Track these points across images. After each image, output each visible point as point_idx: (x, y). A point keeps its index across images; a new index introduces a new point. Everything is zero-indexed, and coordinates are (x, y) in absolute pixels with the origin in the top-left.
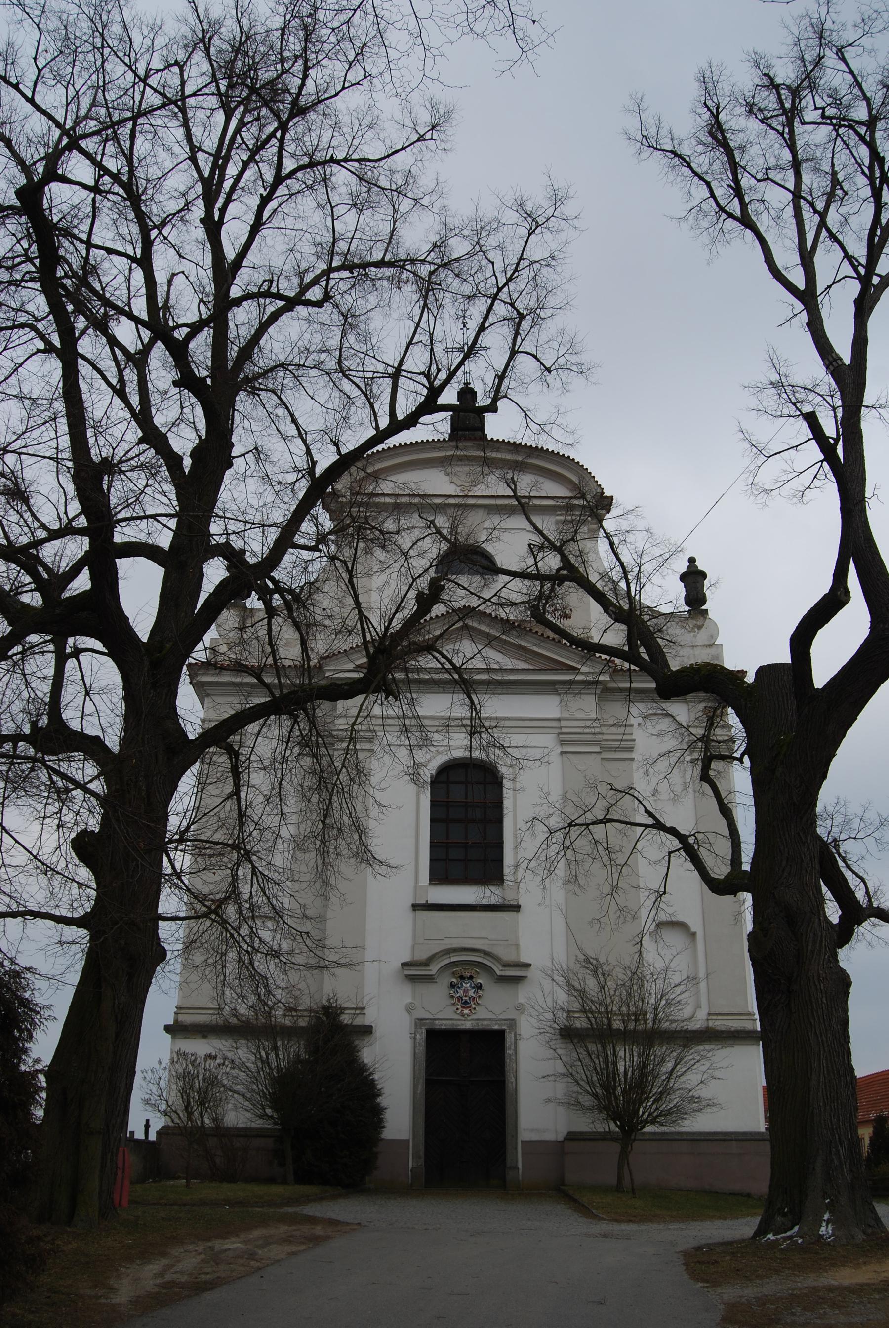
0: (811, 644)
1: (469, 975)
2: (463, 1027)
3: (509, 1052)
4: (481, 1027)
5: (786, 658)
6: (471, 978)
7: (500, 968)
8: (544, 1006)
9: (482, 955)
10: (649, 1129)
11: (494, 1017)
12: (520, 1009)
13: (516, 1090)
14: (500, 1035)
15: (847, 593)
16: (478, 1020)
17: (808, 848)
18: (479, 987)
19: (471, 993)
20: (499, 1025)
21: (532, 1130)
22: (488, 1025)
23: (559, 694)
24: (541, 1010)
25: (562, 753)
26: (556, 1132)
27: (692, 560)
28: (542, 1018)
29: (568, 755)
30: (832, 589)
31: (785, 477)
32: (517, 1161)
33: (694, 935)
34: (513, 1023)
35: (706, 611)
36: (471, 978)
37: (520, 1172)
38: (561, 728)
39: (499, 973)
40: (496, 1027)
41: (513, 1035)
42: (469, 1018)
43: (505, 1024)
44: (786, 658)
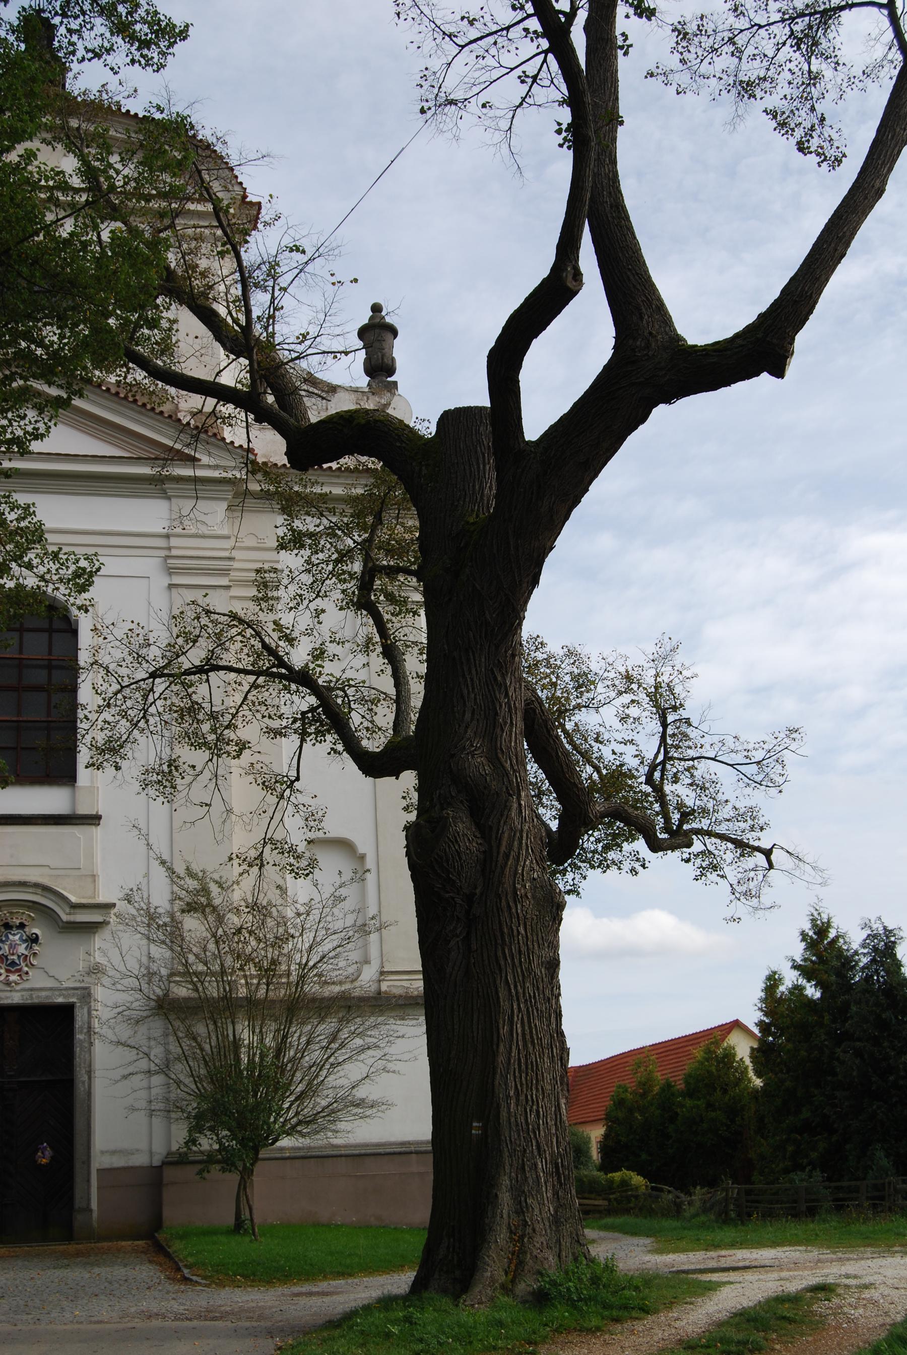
0: (522, 360)
1: (18, 922)
2: (9, 1001)
3: (79, 1036)
4: (36, 1001)
5: (481, 398)
6: (22, 926)
7: (68, 910)
8: (122, 968)
9: (39, 891)
10: (285, 1142)
11: (56, 985)
12: (96, 970)
13: (89, 1094)
14: (65, 1013)
15: (578, 275)
16: (32, 990)
17: (507, 695)
18: (34, 940)
19: (22, 949)
20: (65, 997)
21: (114, 1152)
22: (47, 997)
23: (169, 498)
24: (118, 975)
25: (171, 586)
26: (151, 1153)
27: (376, 309)
28: (119, 987)
29: (181, 590)
30: (554, 269)
31: (487, 77)
32: (89, 1200)
33: (362, 858)
34: (86, 995)
35: (395, 383)
36: (22, 926)
37: (95, 1215)
38: (169, 549)
39: (65, 918)
40: (60, 1000)
41: (86, 1010)
42: (18, 988)
43: (73, 995)
44: (481, 398)
